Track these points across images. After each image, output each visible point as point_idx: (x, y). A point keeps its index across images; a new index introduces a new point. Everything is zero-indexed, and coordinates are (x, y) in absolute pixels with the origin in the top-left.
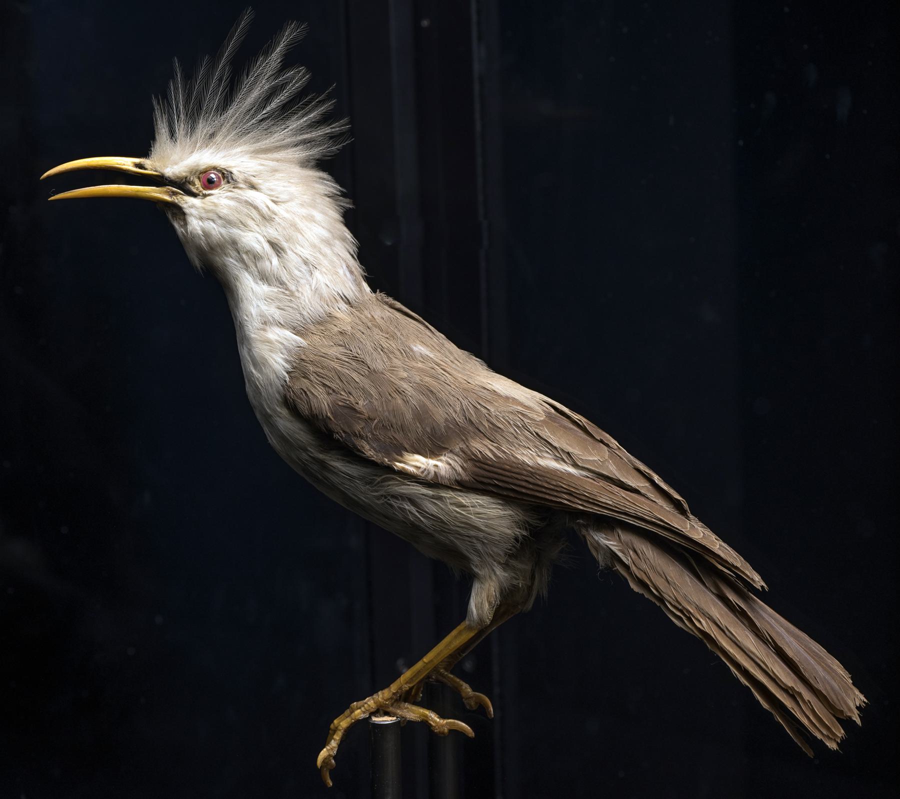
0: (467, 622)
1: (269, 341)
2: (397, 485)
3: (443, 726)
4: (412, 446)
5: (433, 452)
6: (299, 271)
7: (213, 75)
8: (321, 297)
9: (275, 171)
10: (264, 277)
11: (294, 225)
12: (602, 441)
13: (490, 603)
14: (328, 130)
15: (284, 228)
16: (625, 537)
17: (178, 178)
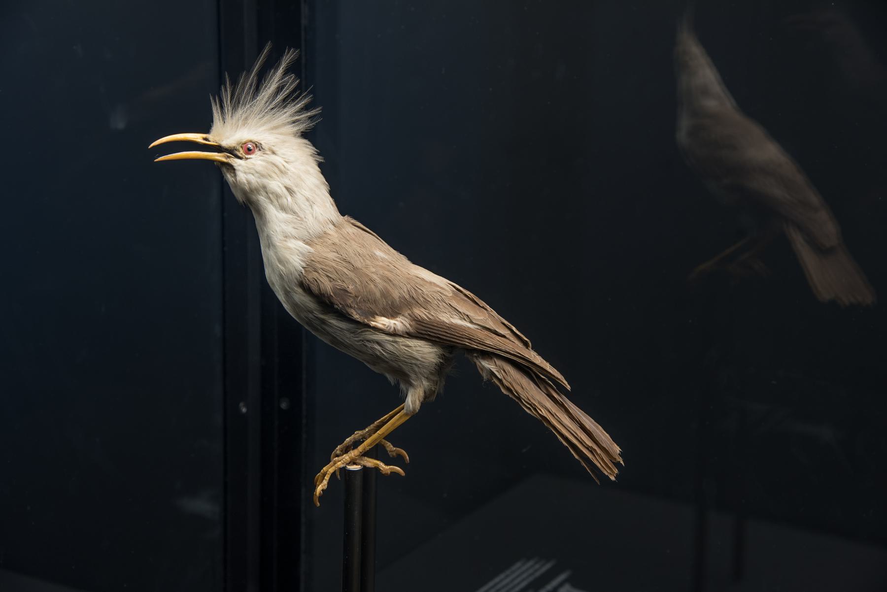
1: (290, 248)
6: (305, 205)
8: (319, 222)
10: (283, 208)
11: (300, 177)
12: (483, 307)
16: (499, 362)
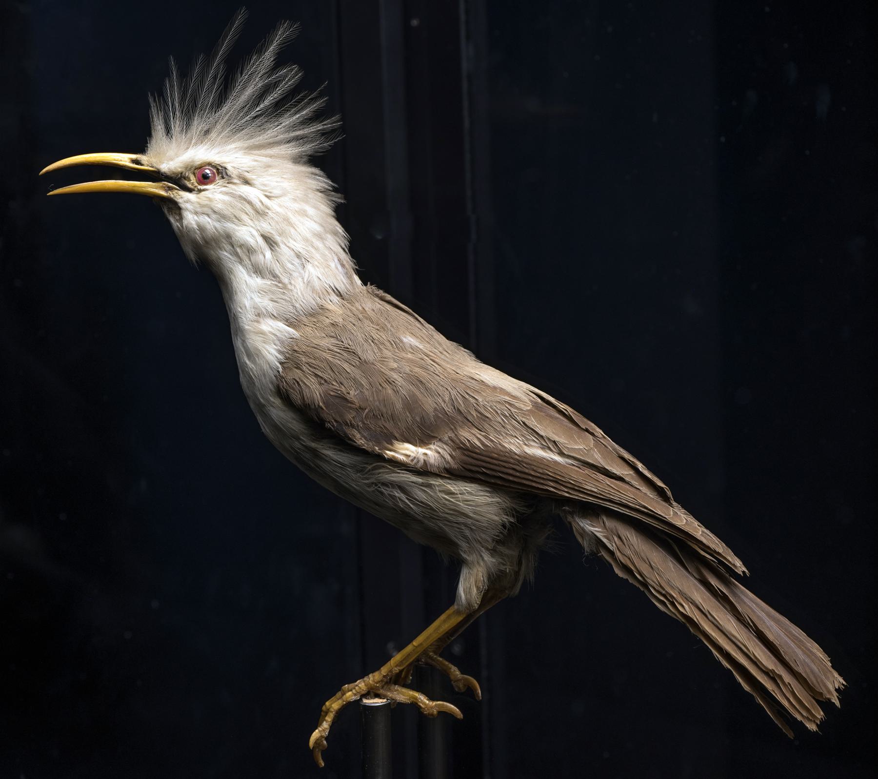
0: (455, 607)
1: (262, 333)
2: (388, 473)
3: (432, 708)
4: (402, 435)
5: (422, 440)
6: (292, 265)
7: (208, 73)
8: (313, 290)
9: (269, 166)
10: (258, 270)
11: (287, 220)
12: (587, 430)
13: (478, 588)
14: (320, 127)
15: (277, 222)
16: (610, 523)
17: (174, 173)
